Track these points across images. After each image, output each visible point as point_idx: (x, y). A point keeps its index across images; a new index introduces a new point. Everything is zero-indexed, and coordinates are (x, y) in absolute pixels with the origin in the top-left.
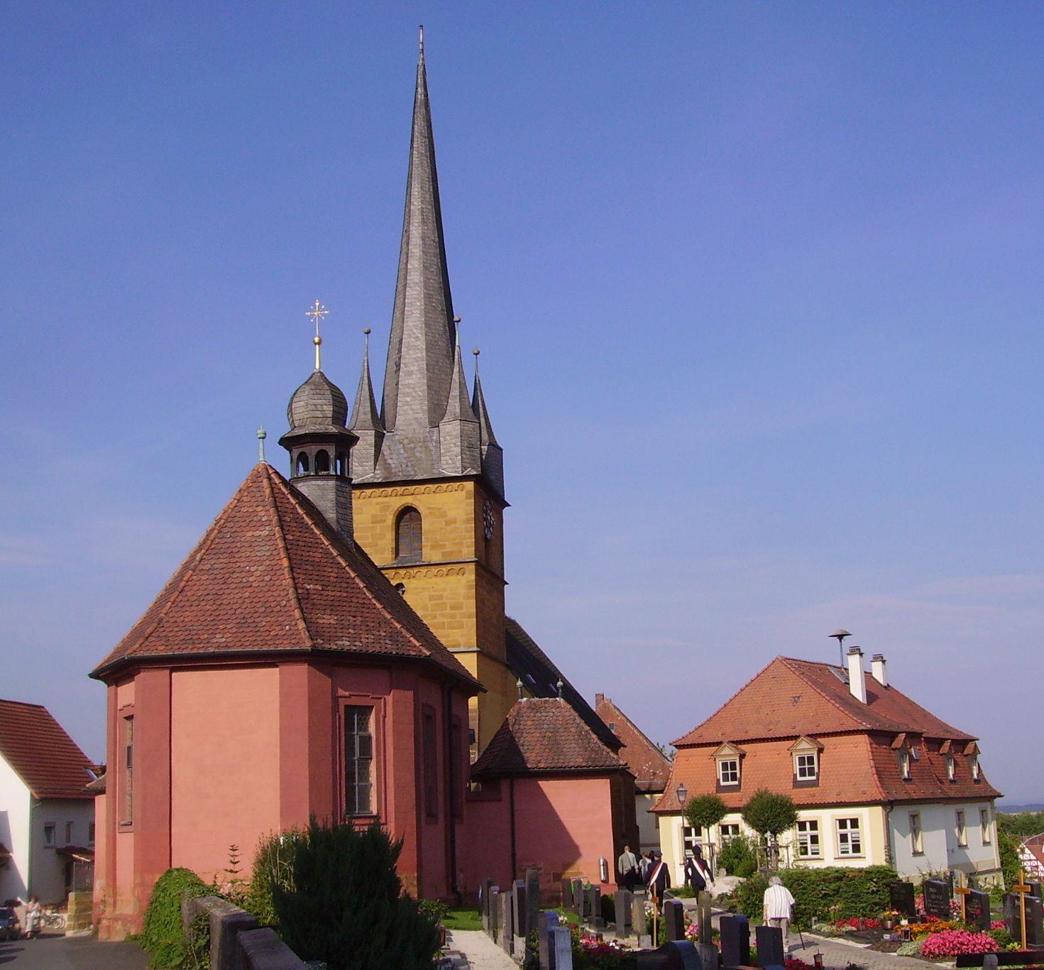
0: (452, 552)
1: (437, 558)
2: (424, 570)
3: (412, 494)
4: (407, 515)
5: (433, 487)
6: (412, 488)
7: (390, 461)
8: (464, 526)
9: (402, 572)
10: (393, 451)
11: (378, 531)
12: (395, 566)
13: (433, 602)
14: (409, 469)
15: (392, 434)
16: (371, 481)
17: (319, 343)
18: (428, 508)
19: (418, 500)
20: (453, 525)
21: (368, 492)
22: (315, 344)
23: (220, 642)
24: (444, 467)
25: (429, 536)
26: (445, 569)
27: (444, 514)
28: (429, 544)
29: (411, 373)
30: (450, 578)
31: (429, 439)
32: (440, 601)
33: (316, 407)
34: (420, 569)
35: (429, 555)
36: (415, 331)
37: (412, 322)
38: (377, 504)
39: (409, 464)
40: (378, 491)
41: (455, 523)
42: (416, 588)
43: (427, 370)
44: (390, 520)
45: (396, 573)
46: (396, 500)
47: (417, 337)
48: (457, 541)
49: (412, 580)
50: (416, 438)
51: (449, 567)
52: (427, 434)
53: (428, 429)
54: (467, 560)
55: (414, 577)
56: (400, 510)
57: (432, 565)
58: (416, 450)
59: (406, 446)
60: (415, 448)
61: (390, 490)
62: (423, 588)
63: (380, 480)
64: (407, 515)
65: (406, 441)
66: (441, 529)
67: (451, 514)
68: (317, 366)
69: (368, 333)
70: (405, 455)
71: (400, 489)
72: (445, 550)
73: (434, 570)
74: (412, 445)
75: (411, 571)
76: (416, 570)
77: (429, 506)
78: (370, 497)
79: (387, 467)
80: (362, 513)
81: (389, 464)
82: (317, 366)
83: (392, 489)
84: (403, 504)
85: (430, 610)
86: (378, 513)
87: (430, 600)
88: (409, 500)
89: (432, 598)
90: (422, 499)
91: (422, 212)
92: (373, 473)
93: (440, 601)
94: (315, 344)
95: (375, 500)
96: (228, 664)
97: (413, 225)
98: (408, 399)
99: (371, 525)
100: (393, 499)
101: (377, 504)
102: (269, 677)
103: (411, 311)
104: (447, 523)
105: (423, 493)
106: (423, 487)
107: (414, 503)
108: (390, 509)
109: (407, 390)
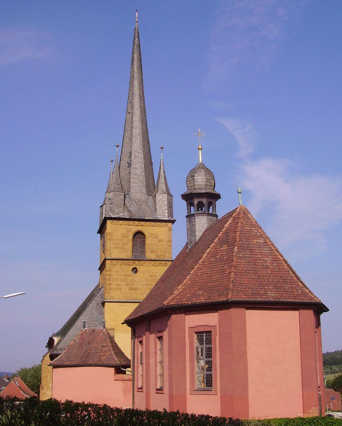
0: (161, 255)
1: (153, 257)
2: (147, 262)
3: (142, 226)
4: (139, 235)
5: (153, 223)
6: (142, 223)
7: (130, 209)
8: (167, 244)
9: (137, 262)
10: (131, 204)
11: (125, 241)
12: (134, 259)
13: (151, 278)
14: (141, 214)
15: (129, 196)
16: (123, 217)
17: (201, 149)
18: (150, 233)
19: (145, 229)
20: (162, 243)
21: (121, 222)
22: (199, 149)
23: (271, 296)
24: (158, 215)
25: (150, 247)
26: (158, 263)
27: (157, 237)
28: (150, 250)
29: (137, 168)
30: (159, 267)
31: (148, 201)
32: (155, 278)
33: (208, 180)
34: (146, 262)
35: (149, 255)
36: (138, 149)
37: (136, 145)
38: (125, 228)
39: (140, 211)
40: (126, 222)
41: (162, 241)
42: (143, 271)
43: (145, 168)
44: (131, 236)
45: (133, 263)
46: (135, 227)
47: (139, 152)
48: (163, 250)
49: (141, 267)
50: (141, 199)
51: (160, 262)
52: (146, 198)
53: (146, 196)
54: (169, 260)
55: (142, 265)
56: (135, 232)
57: (152, 260)
58: (142, 205)
59: (137, 202)
60: (141, 204)
61: (131, 222)
62: (147, 271)
63: (128, 217)
64: (139, 235)
65: (136, 200)
66: (156, 244)
67: (161, 237)
68: (201, 160)
69: (162, 148)
70: (138, 207)
71: (137, 223)
72: (157, 254)
73: (153, 263)
74: (140, 202)
75: (141, 262)
76: (143, 262)
77: (149, 232)
78: (121, 225)
79: (129, 211)
80: (117, 232)
81: (130, 210)
82: (201, 160)
83: (133, 222)
84: (137, 230)
85: (149, 282)
86: (125, 233)
87: (149, 277)
88: (140, 228)
89: (150, 276)
90: (147, 229)
91: (140, 94)
92: (123, 213)
93: (155, 278)
94: (199, 149)
95: (124, 226)
96: (278, 308)
97: (135, 100)
98: (136, 180)
99: (121, 238)
100: (133, 227)
101: (125, 228)
102: (294, 315)
103: (136, 139)
104: (159, 241)
105: (148, 226)
106: (148, 223)
107: (142, 230)
108: (131, 231)
109: (134, 176)
